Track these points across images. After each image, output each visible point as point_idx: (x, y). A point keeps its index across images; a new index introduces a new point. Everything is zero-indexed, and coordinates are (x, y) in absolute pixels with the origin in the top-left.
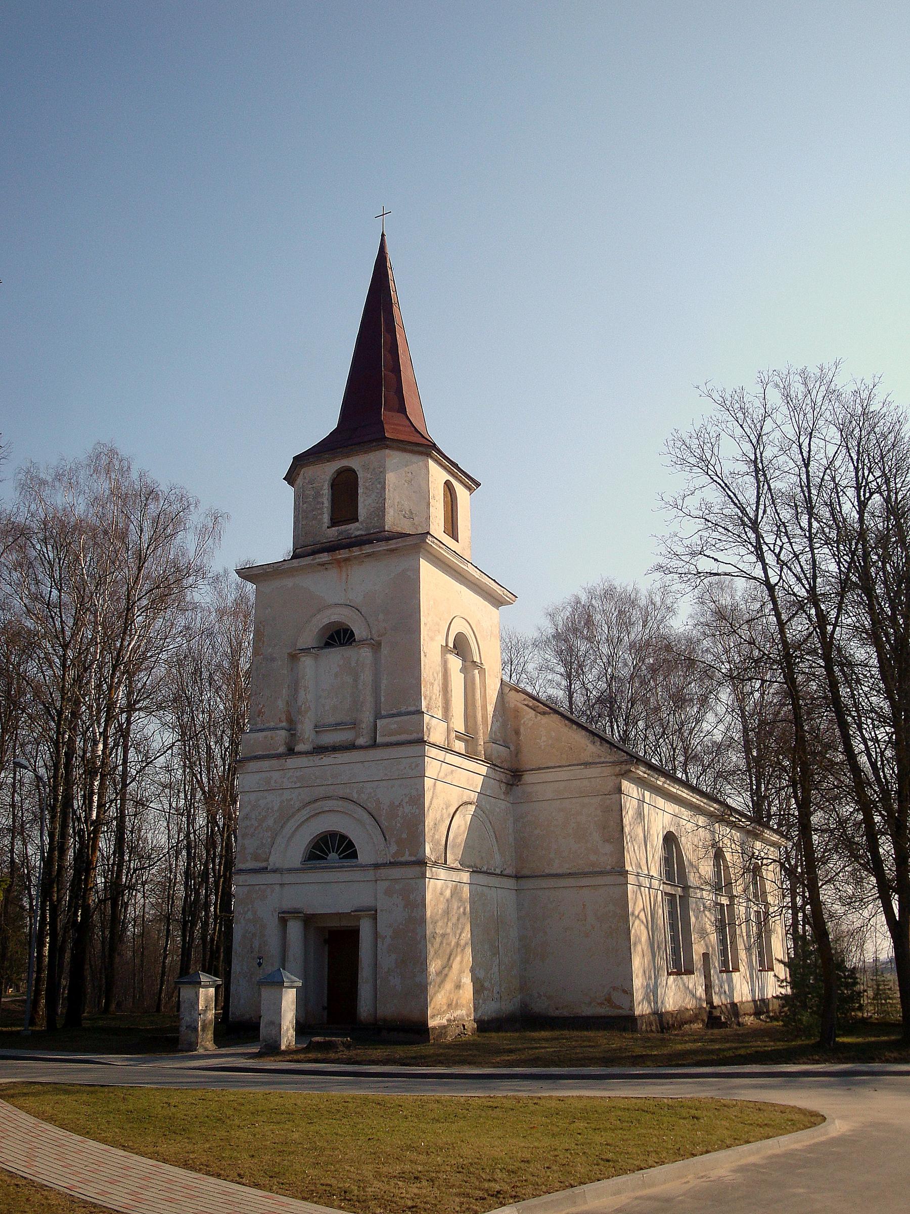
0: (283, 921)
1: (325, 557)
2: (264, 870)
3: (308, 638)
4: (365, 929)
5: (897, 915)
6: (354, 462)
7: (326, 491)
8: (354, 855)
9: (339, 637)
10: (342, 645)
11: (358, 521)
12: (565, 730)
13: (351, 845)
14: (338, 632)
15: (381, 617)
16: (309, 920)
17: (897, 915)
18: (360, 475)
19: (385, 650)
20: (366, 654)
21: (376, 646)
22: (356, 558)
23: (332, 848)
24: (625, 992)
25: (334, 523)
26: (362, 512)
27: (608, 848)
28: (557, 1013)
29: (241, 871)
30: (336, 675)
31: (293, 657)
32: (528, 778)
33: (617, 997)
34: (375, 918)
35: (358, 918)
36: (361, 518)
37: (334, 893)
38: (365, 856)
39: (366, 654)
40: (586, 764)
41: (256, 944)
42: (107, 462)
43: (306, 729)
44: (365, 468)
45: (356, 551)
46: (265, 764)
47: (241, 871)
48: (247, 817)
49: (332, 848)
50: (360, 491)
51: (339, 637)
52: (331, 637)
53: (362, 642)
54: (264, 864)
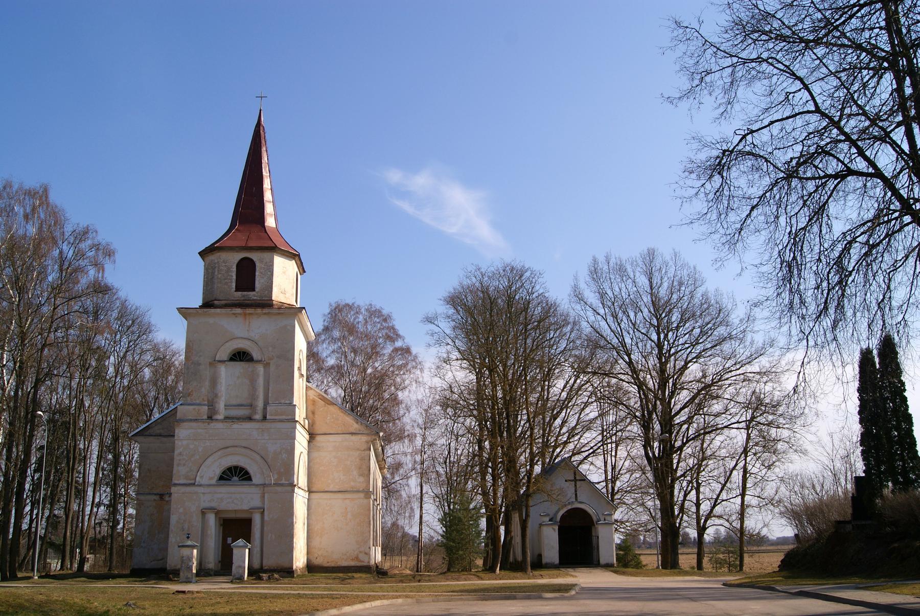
0: (203, 513)
1: (239, 311)
2: (194, 484)
3: (224, 354)
4: (257, 519)
5: (877, 360)
6: (254, 256)
7: (235, 267)
8: (250, 479)
9: (240, 356)
10: (241, 360)
11: (253, 289)
12: (342, 414)
13: (247, 473)
14: (239, 353)
15: (270, 349)
16: (218, 513)
17: (877, 360)
18: (258, 264)
19: (272, 368)
20: (260, 369)
21: (267, 365)
22: (257, 314)
23: (236, 474)
24: (366, 553)
25: (237, 289)
26: (258, 285)
27: (362, 479)
28: (328, 565)
29: (176, 485)
30: (238, 377)
31: (214, 363)
32: (318, 438)
33: (362, 557)
34: (262, 513)
35: (252, 513)
36: (257, 290)
37: (237, 499)
38: (256, 480)
39: (260, 369)
40: (352, 434)
41: (186, 526)
42: (40, 196)
43: (221, 406)
44: (261, 261)
45: (259, 311)
46: (194, 424)
47: (176, 485)
48: (180, 454)
49: (236, 474)
50: (257, 274)
51: (240, 356)
52: (234, 355)
53: (259, 361)
54: (192, 482)
